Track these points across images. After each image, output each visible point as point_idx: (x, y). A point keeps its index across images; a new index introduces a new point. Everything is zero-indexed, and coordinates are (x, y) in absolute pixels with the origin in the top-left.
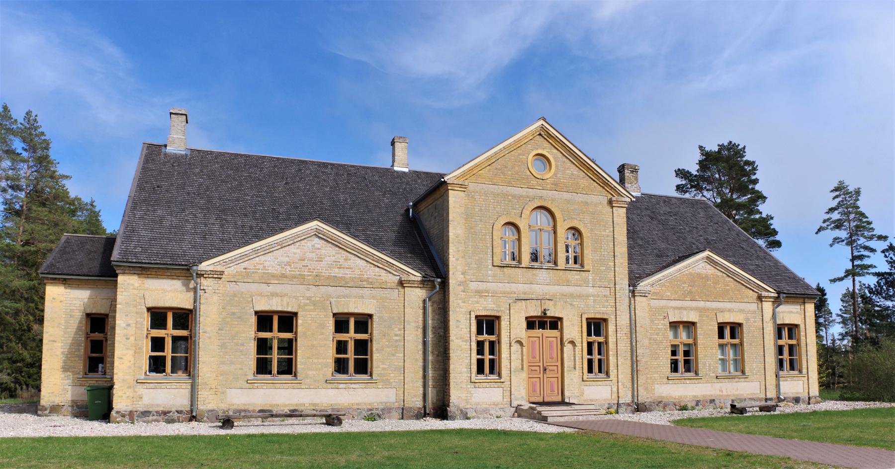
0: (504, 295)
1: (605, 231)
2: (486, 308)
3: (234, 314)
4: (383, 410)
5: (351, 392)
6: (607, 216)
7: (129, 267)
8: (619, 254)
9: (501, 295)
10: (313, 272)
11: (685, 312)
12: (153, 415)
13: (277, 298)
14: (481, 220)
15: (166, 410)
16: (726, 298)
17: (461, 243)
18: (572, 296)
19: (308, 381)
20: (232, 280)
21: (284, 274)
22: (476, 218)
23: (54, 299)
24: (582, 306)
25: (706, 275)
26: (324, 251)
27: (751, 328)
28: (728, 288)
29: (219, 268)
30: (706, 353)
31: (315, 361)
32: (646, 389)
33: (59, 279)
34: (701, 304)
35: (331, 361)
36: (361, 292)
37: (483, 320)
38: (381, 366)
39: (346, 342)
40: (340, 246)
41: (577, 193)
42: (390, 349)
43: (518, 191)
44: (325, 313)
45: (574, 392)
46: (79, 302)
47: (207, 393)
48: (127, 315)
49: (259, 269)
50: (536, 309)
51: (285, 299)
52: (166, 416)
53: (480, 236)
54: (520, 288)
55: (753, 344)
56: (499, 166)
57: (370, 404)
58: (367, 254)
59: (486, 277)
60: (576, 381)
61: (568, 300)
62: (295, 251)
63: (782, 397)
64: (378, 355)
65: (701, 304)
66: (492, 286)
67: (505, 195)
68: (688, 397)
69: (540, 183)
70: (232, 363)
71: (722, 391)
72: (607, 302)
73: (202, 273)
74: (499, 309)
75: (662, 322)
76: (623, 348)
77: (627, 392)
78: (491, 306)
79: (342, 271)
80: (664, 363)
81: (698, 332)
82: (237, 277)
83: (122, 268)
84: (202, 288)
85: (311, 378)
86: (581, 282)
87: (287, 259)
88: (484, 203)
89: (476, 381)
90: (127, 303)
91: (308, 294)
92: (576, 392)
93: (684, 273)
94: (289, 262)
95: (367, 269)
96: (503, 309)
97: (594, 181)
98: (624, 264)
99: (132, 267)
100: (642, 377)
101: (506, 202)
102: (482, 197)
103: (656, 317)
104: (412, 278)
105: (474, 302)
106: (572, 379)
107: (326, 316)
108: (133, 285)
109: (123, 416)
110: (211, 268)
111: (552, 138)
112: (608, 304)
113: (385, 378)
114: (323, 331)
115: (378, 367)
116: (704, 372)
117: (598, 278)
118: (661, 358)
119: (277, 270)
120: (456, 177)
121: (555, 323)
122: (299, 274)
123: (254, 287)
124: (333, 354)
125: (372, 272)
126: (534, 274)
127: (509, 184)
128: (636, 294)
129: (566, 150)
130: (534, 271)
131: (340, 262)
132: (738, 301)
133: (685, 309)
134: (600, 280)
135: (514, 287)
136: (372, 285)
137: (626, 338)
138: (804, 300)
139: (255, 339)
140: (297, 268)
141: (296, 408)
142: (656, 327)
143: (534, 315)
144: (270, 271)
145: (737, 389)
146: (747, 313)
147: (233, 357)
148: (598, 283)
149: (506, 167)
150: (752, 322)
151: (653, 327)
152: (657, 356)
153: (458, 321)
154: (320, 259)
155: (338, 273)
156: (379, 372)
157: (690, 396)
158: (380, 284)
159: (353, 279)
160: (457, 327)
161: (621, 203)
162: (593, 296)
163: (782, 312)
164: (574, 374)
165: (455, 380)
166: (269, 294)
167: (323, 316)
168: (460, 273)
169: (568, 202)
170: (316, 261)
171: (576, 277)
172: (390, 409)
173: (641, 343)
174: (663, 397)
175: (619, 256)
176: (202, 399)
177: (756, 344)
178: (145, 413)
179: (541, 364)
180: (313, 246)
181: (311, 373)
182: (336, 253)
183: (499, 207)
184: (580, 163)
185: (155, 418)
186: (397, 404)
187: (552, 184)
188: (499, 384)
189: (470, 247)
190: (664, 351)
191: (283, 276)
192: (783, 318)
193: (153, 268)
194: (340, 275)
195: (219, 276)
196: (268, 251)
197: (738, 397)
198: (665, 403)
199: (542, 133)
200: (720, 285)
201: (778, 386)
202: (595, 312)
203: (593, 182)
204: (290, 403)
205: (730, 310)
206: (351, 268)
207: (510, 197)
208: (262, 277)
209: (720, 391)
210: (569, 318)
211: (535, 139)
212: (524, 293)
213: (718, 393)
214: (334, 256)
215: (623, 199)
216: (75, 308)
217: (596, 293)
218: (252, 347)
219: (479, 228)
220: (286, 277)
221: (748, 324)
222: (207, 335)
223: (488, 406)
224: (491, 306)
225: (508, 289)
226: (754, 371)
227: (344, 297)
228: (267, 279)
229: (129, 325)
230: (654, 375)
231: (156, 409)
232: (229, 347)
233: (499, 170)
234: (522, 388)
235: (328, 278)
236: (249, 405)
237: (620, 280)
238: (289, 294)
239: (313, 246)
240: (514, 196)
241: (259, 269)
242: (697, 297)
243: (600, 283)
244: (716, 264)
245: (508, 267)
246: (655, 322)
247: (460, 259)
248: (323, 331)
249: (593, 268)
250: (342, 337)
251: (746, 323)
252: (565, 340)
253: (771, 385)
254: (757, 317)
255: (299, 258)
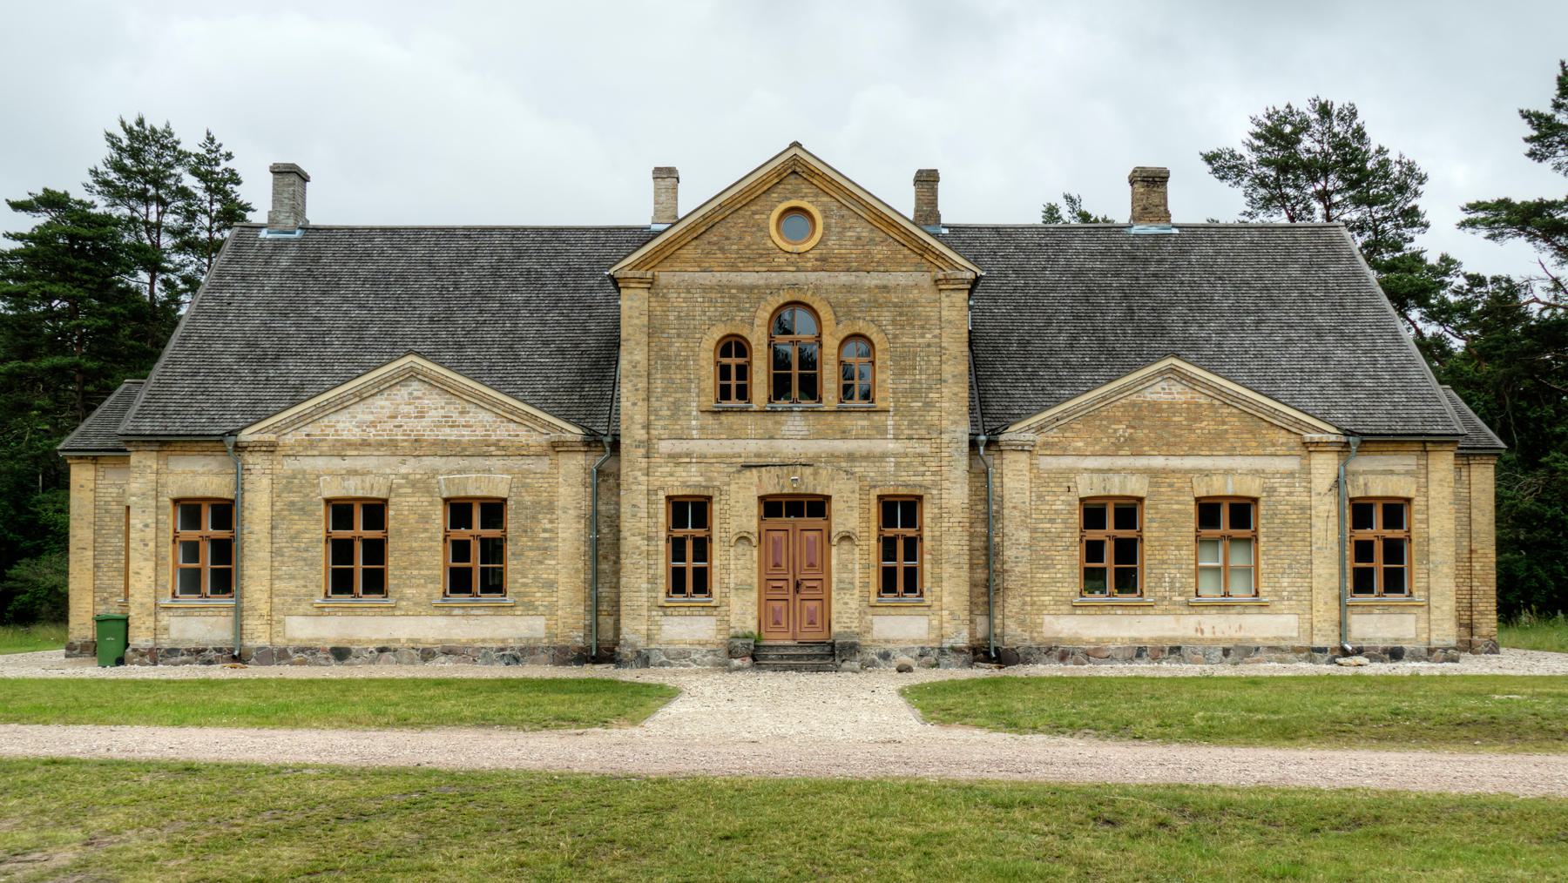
0: (719, 460)
1: (923, 336)
2: (686, 481)
3: (293, 503)
4: (522, 650)
5: (473, 621)
6: (928, 309)
7: (144, 441)
8: (950, 376)
9: (714, 460)
10: (409, 435)
11: (1116, 479)
12: (183, 655)
13: (355, 478)
14: (679, 336)
15: (201, 647)
16: (1219, 448)
17: (641, 376)
18: (851, 457)
19: (404, 603)
20: (290, 453)
21: (366, 440)
22: (671, 331)
23: (82, 486)
24: (872, 474)
25: (1171, 403)
26: (426, 402)
27: (1280, 507)
28: (1225, 427)
29: (270, 437)
30: (1165, 557)
31: (415, 572)
32: (1022, 623)
33: (87, 457)
34: (1158, 462)
35: (441, 573)
36: (488, 463)
37: (897, 502)
38: (520, 581)
39: (1371, 543)
40: (452, 391)
41: (868, 272)
42: (537, 553)
43: (749, 278)
44: (430, 499)
45: (849, 625)
46: (117, 491)
47: (256, 623)
48: (144, 512)
49: (328, 435)
50: (778, 483)
51: (368, 479)
52: (198, 654)
53: (678, 363)
54: (751, 447)
55: (1283, 539)
56: (715, 239)
57: (503, 641)
58: (495, 404)
59: (686, 432)
60: (854, 606)
61: (844, 464)
62: (383, 403)
63: (1349, 647)
64: (515, 562)
65: (1158, 462)
66: (698, 446)
67: (722, 288)
68: (1119, 640)
69: (793, 260)
70: (293, 577)
71: (1202, 631)
72: (924, 465)
73: (245, 444)
74: (709, 484)
75: (1062, 498)
76: (953, 548)
77: (961, 627)
78: (695, 479)
79: (455, 431)
80: (1066, 576)
81: (1146, 516)
82: (297, 449)
83: (134, 444)
84: (246, 467)
85: (408, 599)
86: (870, 432)
87: (371, 418)
88: (684, 305)
89: (666, 604)
90: (144, 494)
91: (403, 470)
92: (854, 625)
93: (1118, 403)
94: (374, 422)
95: (496, 425)
96: (718, 484)
97: (904, 245)
98: (960, 395)
99: (148, 441)
100: (1014, 601)
101: (727, 300)
102: (683, 295)
103: (1049, 489)
104: (569, 437)
105: (665, 474)
106: (846, 604)
107: (431, 503)
108: (150, 467)
109: (143, 655)
110: (256, 437)
111: (817, 177)
112: (926, 469)
113: (526, 599)
114: (427, 526)
115: (515, 581)
116: (1159, 594)
117: (906, 423)
118: (1060, 567)
119: (355, 435)
120: (631, 267)
121: (818, 506)
122: (390, 440)
123: (321, 463)
124: (445, 561)
125: (503, 431)
126: (777, 423)
127: (734, 268)
128: (1002, 448)
129: (845, 196)
130: (778, 417)
131: (451, 417)
132: (1249, 453)
133: (1117, 472)
134: (910, 426)
135: (739, 446)
136: (506, 450)
137: (960, 529)
138: (1425, 447)
139: (327, 540)
140: (385, 430)
141: (386, 645)
142: (1048, 507)
143: (775, 492)
144: (345, 438)
145: (1240, 627)
146: (1269, 476)
147: (292, 568)
148: (906, 432)
149: (727, 238)
150: (1282, 494)
151: (1041, 507)
152: (1049, 562)
153: (634, 506)
154: (421, 415)
155: (451, 435)
156: (516, 590)
157: (1122, 639)
158: (519, 448)
159: (473, 444)
160: (634, 516)
161: (956, 282)
162: (895, 455)
163: (1365, 473)
164: (852, 595)
165: (629, 603)
166: (344, 472)
167: (427, 504)
168: (639, 426)
169: (849, 289)
170: (416, 417)
171: (861, 423)
172: (534, 648)
173: (1014, 538)
174: (1060, 640)
175: (950, 381)
176: (249, 631)
177: (1291, 539)
178: (172, 652)
179: (790, 577)
180: (411, 394)
181: (408, 592)
182: (446, 403)
183: (712, 309)
184: (873, 216)
185: (184, 658)
186: (546, 641)
187: (817, 260)
188: (709, 610)
189: (659, 381)
190: (1067, 553)
191: (365, 443)
192: (1366, 485)
193: (177, 441)
194: (453, 438)
195: (272, 449)
196: (341, 405)
197: (1240, 645)
198: (1063, 651)
199: (798, 170)
200: (1205, 423)
201: (1342, 625)
202: (898, 482)
203: (902, 248)
204: (379, 637)
205: (1227, 472)
206: (471, 426)
207: (733, 291)
208: (334, 446)
209: (1197, 630)
210: (842, 497)
211: (785, 182)
212: (758, 455)
213: (1191, 633)
214: (443, 408)
215: (960, 275)
216: (110, 499)
217: (902, 450)
218: (1078, 553)
219: (675, 349)
220: (369, 445)
221: (1273, 499)
222: (255, 536)
223: (688, 646)
224: (695, 479)
225: (728, 451)
226: (1285, 594)
227: (459, 472)
228: (341, 449)
229: (146, 526)
230: (1042, 598)
231: (188, 646)
232: (287, 554)
233: (715, 244)
234: (750, 617)
235: (434, 443)
236: (318, 640)
237: (952, 424)
238: (375, 471)
239: (411, 394)
240: (741, 288)
241: (328, 435)
242: (1146, 448)
243: (910, 432)
244: (1194, 382)
245: (727, 411)
246: (1047, 498)
247: (639, 404)
248: (427, 526)
249: (895, 406)
250: (462, 534)
251: (1269, 496)
252: (833, 534)
253: (1325, 621)
254: (1297, 485)
255: (388, 415)
